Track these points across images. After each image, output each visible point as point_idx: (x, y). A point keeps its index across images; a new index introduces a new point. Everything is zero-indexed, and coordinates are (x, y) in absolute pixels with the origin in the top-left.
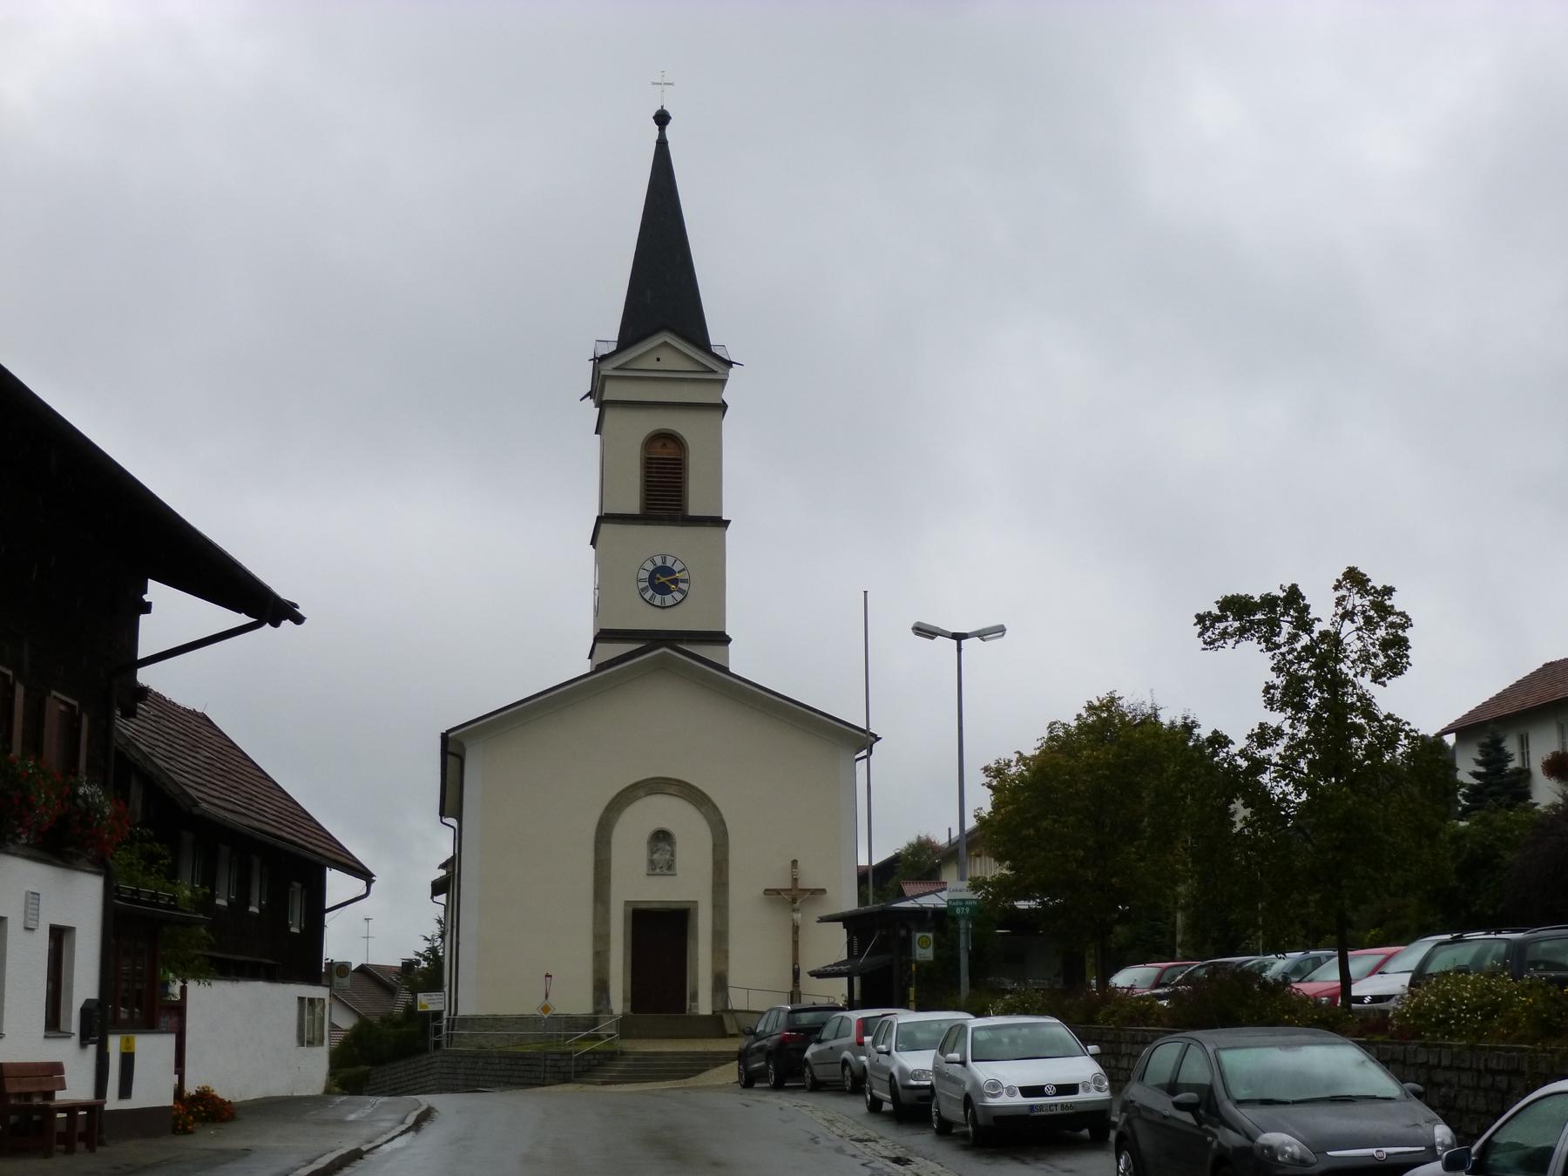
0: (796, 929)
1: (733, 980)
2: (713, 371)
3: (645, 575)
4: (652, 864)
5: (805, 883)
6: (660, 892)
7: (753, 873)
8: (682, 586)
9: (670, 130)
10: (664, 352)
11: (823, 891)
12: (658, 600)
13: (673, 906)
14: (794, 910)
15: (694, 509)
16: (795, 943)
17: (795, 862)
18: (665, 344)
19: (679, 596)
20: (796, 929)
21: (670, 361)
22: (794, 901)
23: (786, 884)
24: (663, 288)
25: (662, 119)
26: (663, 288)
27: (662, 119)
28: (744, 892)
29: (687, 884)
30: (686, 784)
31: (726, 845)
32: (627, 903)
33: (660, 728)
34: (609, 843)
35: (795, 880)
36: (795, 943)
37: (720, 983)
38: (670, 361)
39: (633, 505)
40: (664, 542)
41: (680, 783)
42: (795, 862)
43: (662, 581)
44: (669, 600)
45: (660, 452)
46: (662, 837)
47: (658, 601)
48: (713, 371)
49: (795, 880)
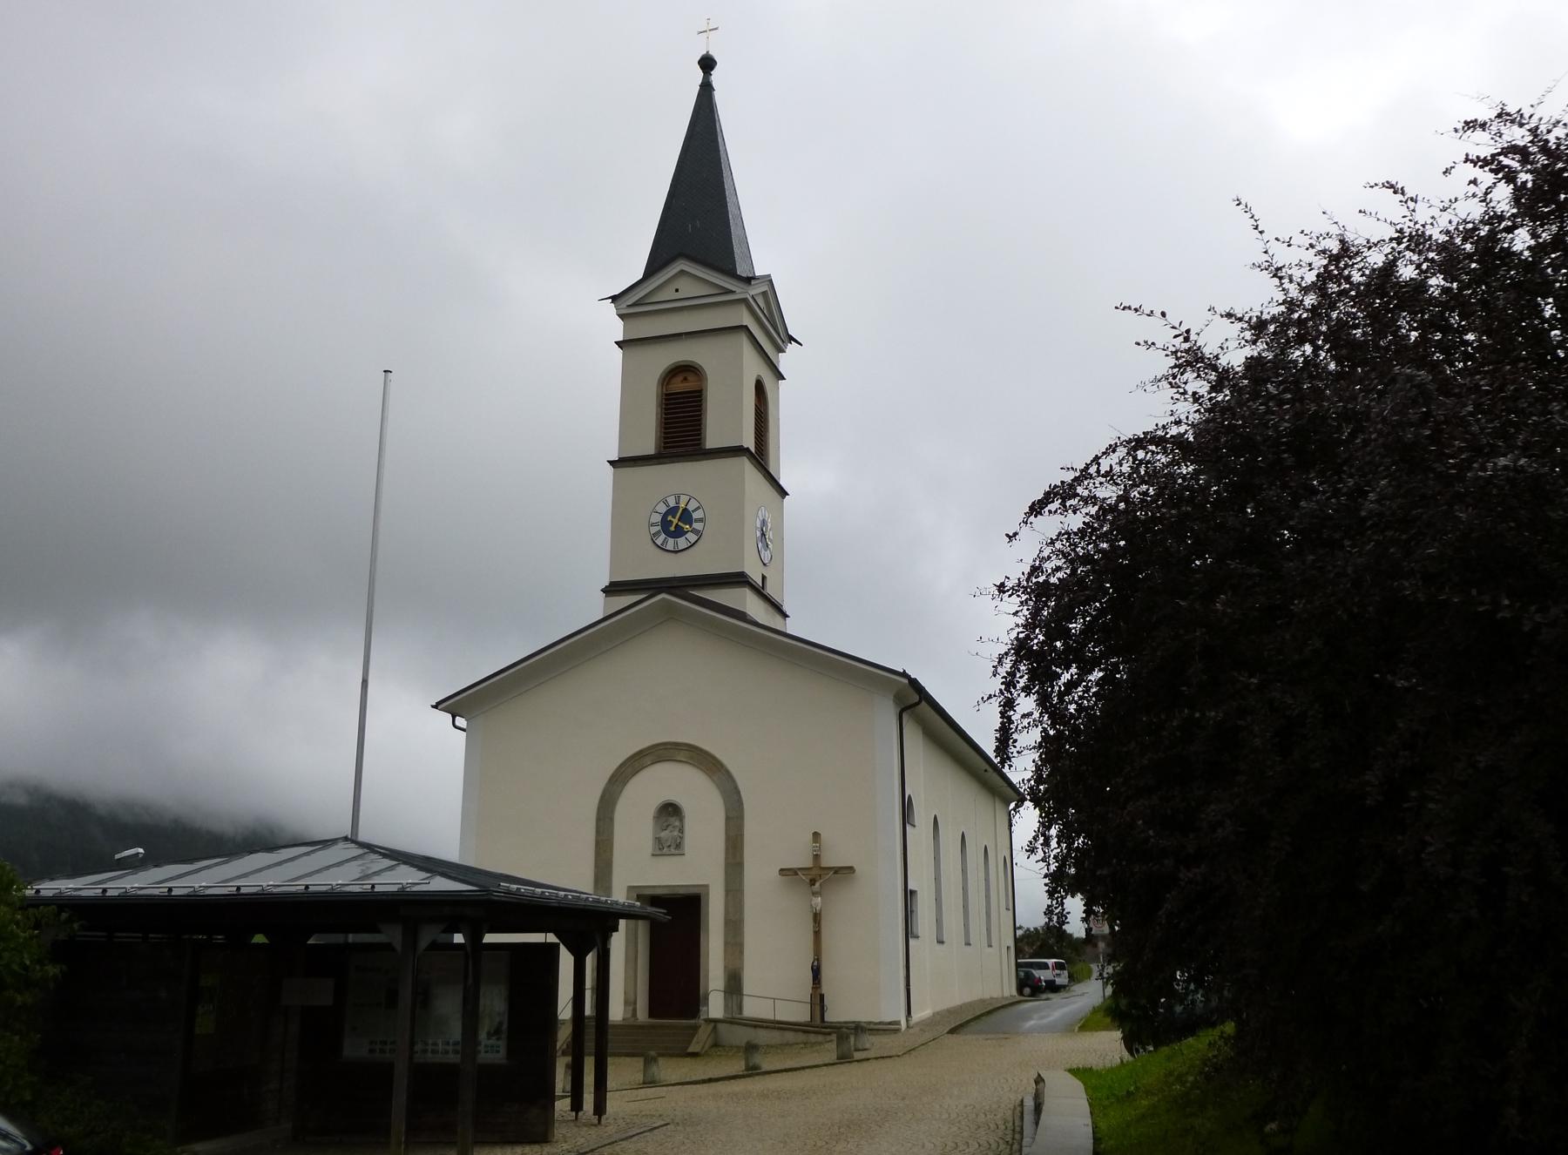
0: (817, 918)
1: (748, 987)
2: (732, 292)
3: (657, 518)
4: (659, 842)
5: (829, 861)
6: (669, 875)
7: (772, 847)
8: (696, 526)
9: (716, 77)
10: (689, 280)
11: (851, 869)
12: (670, 544)
13: (682, 891)
14: (815, 894)
15: (711, 442)
16: (817, 934)
17: (816, 835)
18: (682, 272)
19: (692, 537)
20: (817, 918)
21: (688, 289)
22: (813, 882)
23: (809, 863)
24: (698, 217)
25: (707, 64)
26: (698, 217)
27: (707, 64)
28: (760, 873)
29: (696, 867)
30: (696, 748)
31: (741, 817)
32: (707, 886)
33: (676, 686)
34: (612, 819)
35: (817, 857)
36: (817, 934)
37: (734, 985)
38: (688, 289)
39: (648, 446)
40: (682, 481)
41: (677, 746)
42: (816, 835)
43: (676, 523)
44: (682, 543)
45: (678, 386)
46: (670, 811)
47: (670, 546)
48: (732, 292)
49: (817, 857)
